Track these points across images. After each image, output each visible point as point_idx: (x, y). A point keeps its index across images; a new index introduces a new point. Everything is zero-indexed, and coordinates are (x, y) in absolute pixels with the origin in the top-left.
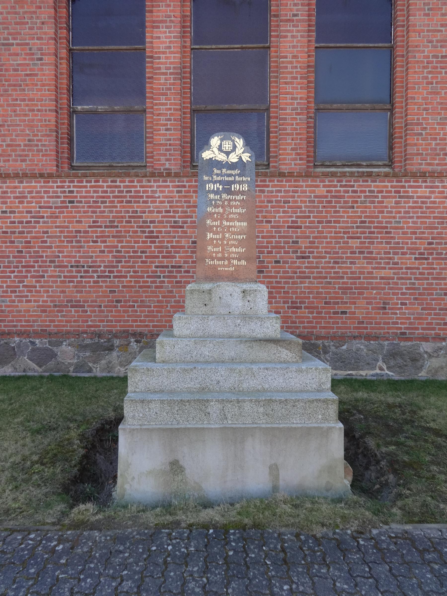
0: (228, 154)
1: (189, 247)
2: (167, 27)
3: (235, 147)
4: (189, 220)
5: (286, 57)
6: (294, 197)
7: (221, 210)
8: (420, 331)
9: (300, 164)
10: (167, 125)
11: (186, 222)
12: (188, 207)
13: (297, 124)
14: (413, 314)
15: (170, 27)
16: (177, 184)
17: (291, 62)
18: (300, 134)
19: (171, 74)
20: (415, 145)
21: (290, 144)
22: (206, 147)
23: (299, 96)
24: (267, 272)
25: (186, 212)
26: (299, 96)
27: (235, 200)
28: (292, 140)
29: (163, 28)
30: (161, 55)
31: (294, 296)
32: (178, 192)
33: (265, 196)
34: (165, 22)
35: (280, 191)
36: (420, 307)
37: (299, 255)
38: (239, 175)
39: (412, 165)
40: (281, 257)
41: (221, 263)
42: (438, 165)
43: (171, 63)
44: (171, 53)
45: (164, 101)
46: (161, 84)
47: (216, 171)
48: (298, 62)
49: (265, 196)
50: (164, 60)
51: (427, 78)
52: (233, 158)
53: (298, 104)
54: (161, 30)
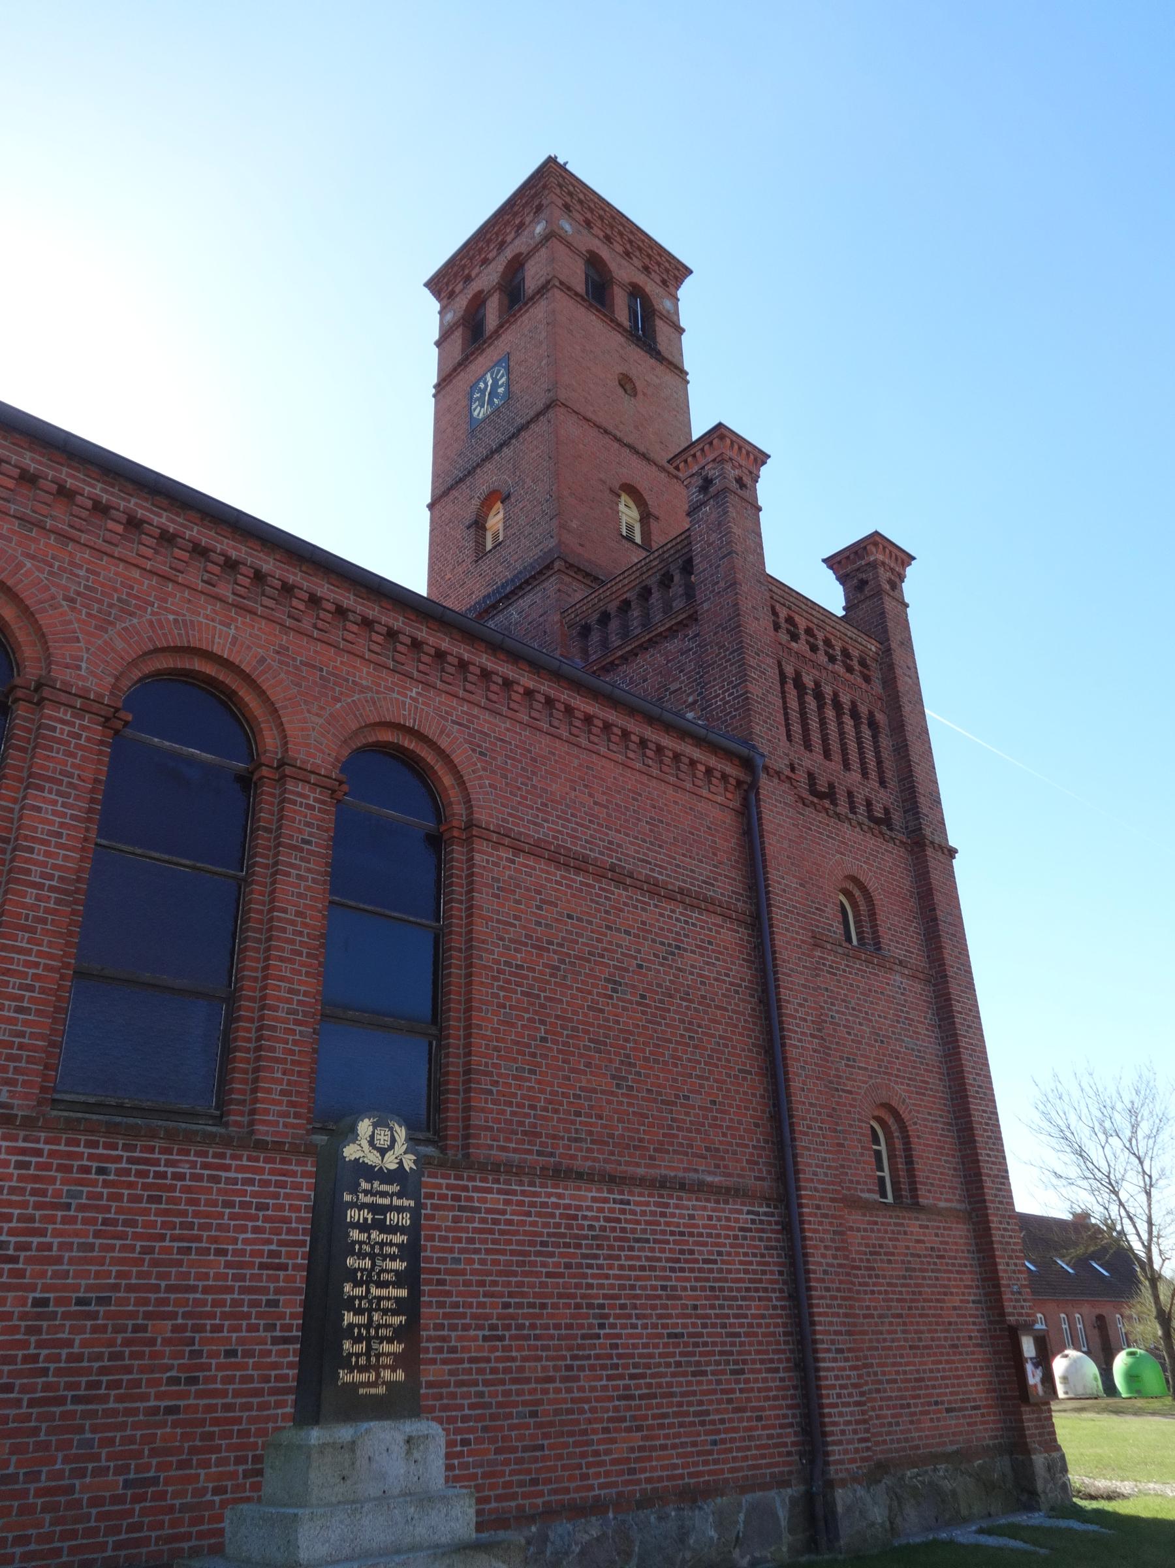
0: (383, 1152)
1: (24, 1316)
2: (60, 793)
3: (393, 1140)
4: (36, 1240)
5: (285, 911)
6: (276, 1196)
7: (367, 1263)
8: (493, 1505)
9: (294, 1126)
10: (21, 998)
11: (26, 1247)
12: (38, 1206)
13: (295, 1042)
14: (481, 1466)
15: (68, 796)
16: (21, 1144)
17: (293, 923)
18: (299, 1063)
19: (52, 889)
20: (483, 1110)
21: (278, 1081)
22: (350, 1136)
23: (302, 988)
24: (207, 1380)
25: (31, 1219)
26: (302, 988)
27: (391, 1244)
28: (284, 1073)
29: (50, 792)
30: (37, 846)
31: (260, 1441)
32: (20, 1165)
33: (219, 1190)
34: (60, 783)
35: (251, 1182)
36: (492, 1447)
37: (278, 1334)
38: (400, 1195)
39: (478, 1146)
40: (241, 1341)
41: (363, 1377)
42: (515, 1150)
43: (55, 867)
44: (59, 846)
45: (24, 945)
46: (24, 906)
47: (364, 1185)
48: (305, 925)
49: (219, 1190)
50: (41, 858)
51: (497, 996)
52: (390, 1162)
53: (300, 1002)
54: (46, 794)
